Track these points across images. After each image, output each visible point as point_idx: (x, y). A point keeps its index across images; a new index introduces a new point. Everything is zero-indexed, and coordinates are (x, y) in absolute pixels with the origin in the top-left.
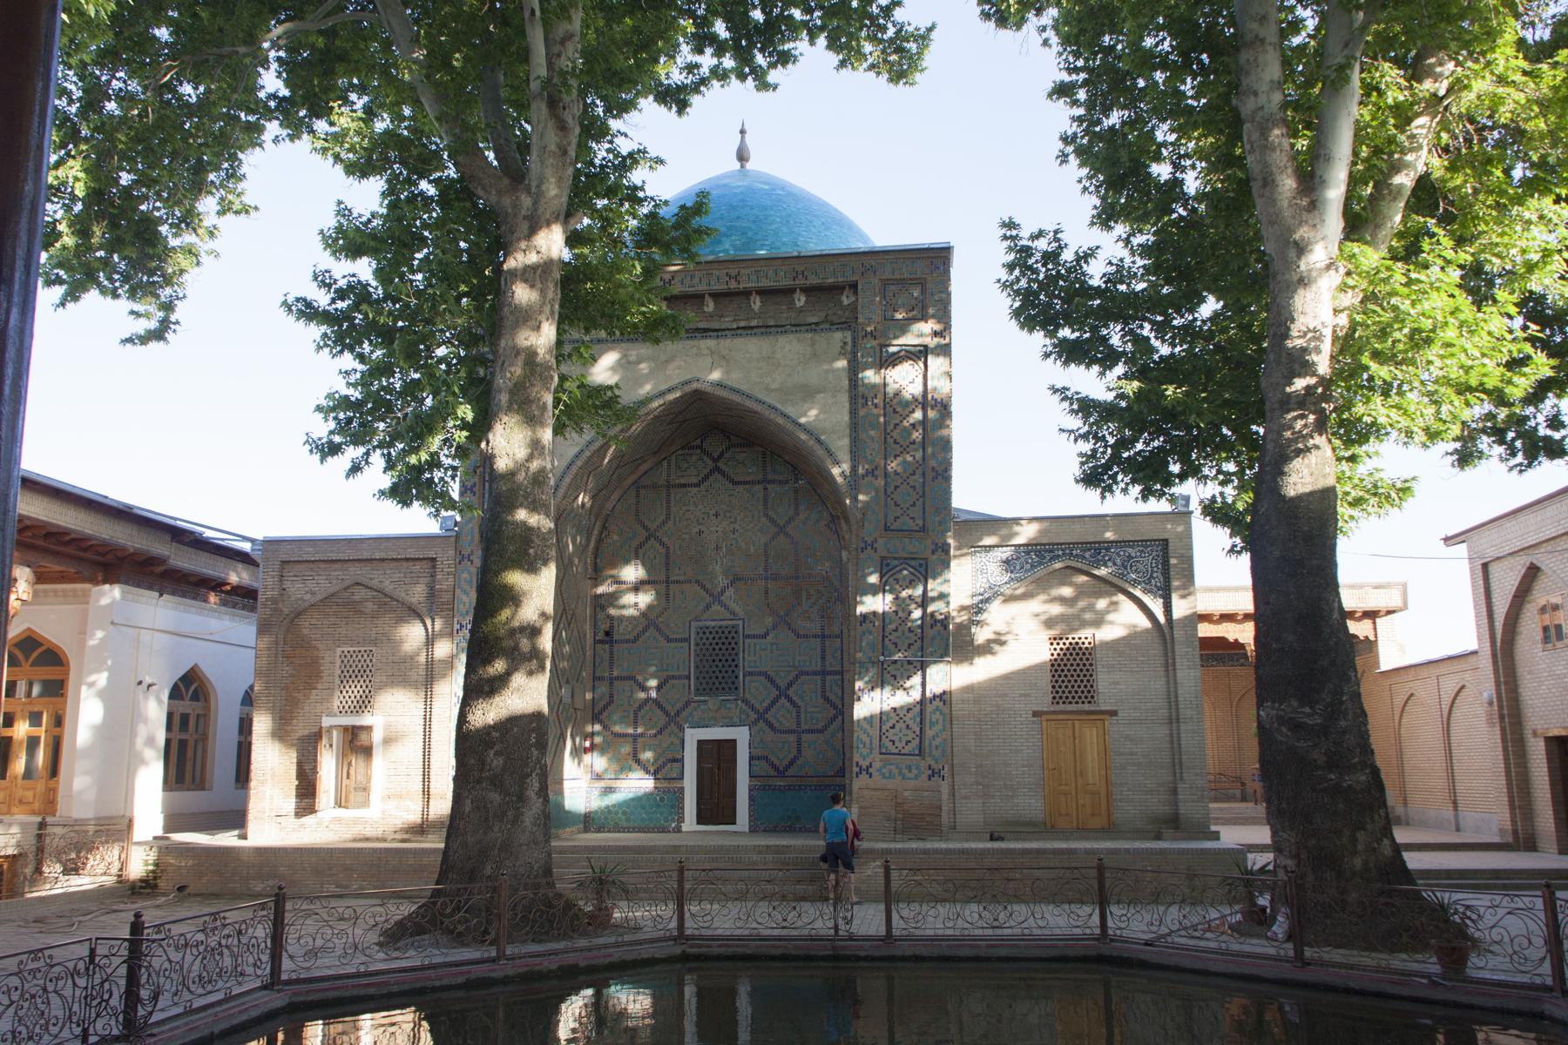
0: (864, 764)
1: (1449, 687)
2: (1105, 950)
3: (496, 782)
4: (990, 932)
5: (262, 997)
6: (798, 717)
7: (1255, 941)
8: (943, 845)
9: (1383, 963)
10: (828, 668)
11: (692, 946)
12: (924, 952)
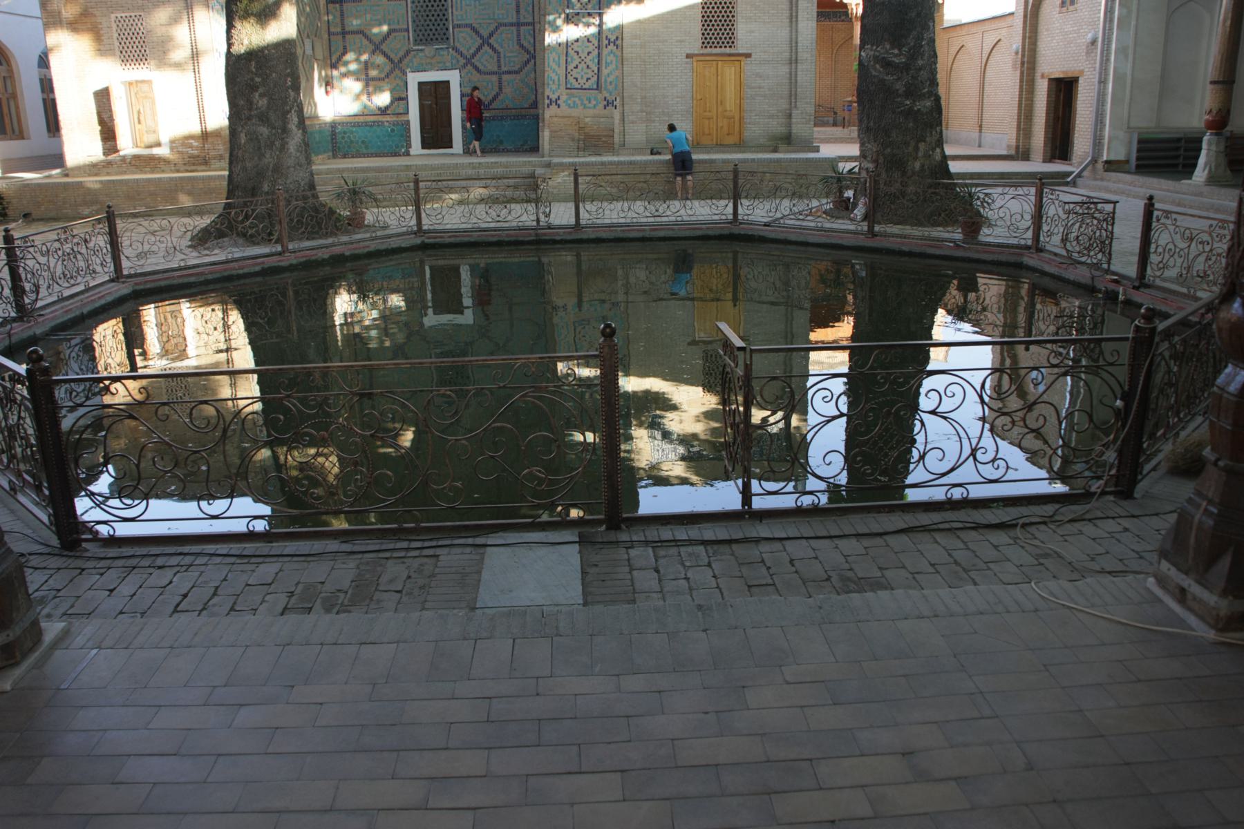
0: (554, 97)
1: (990, 40)
2: (736, 230)
3: (263, 118)
4: (652, 220)
5: (113, 287)
6: (499, 61)
7: (840, 221)
8: (615, 159)
9: (926, 234)
10: (522, 20)
11: (429, 238)
12: (604, 235)
